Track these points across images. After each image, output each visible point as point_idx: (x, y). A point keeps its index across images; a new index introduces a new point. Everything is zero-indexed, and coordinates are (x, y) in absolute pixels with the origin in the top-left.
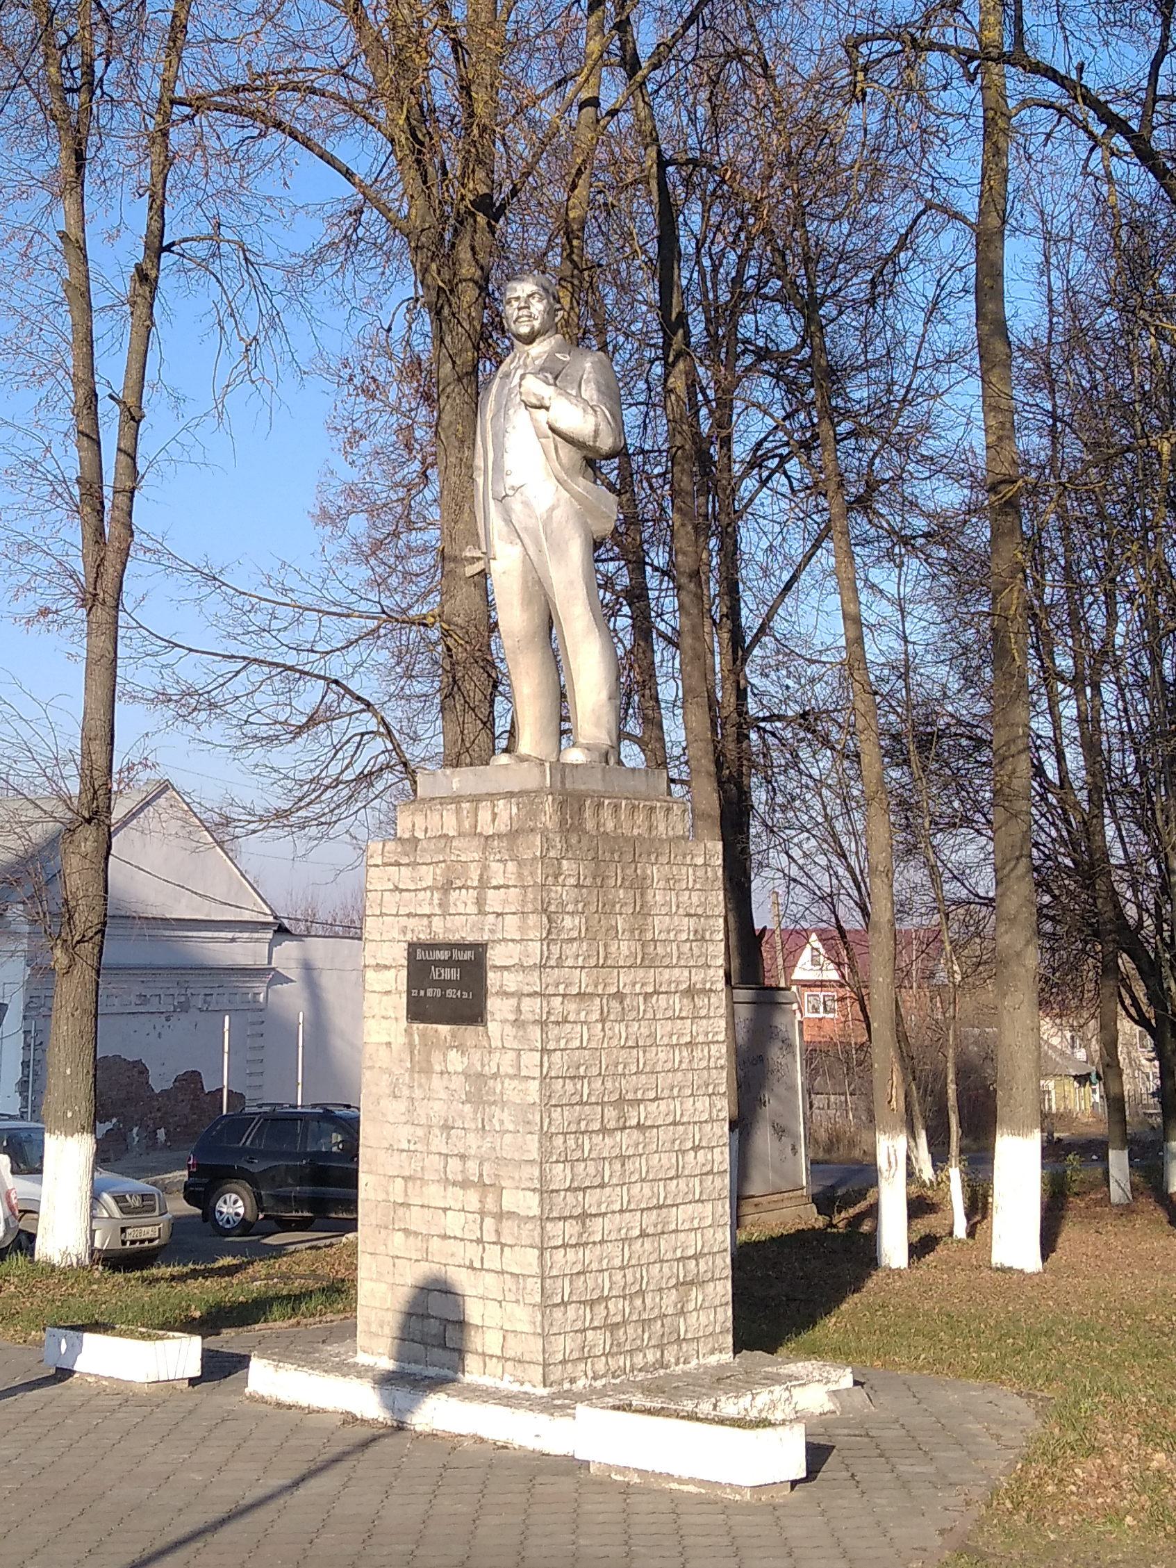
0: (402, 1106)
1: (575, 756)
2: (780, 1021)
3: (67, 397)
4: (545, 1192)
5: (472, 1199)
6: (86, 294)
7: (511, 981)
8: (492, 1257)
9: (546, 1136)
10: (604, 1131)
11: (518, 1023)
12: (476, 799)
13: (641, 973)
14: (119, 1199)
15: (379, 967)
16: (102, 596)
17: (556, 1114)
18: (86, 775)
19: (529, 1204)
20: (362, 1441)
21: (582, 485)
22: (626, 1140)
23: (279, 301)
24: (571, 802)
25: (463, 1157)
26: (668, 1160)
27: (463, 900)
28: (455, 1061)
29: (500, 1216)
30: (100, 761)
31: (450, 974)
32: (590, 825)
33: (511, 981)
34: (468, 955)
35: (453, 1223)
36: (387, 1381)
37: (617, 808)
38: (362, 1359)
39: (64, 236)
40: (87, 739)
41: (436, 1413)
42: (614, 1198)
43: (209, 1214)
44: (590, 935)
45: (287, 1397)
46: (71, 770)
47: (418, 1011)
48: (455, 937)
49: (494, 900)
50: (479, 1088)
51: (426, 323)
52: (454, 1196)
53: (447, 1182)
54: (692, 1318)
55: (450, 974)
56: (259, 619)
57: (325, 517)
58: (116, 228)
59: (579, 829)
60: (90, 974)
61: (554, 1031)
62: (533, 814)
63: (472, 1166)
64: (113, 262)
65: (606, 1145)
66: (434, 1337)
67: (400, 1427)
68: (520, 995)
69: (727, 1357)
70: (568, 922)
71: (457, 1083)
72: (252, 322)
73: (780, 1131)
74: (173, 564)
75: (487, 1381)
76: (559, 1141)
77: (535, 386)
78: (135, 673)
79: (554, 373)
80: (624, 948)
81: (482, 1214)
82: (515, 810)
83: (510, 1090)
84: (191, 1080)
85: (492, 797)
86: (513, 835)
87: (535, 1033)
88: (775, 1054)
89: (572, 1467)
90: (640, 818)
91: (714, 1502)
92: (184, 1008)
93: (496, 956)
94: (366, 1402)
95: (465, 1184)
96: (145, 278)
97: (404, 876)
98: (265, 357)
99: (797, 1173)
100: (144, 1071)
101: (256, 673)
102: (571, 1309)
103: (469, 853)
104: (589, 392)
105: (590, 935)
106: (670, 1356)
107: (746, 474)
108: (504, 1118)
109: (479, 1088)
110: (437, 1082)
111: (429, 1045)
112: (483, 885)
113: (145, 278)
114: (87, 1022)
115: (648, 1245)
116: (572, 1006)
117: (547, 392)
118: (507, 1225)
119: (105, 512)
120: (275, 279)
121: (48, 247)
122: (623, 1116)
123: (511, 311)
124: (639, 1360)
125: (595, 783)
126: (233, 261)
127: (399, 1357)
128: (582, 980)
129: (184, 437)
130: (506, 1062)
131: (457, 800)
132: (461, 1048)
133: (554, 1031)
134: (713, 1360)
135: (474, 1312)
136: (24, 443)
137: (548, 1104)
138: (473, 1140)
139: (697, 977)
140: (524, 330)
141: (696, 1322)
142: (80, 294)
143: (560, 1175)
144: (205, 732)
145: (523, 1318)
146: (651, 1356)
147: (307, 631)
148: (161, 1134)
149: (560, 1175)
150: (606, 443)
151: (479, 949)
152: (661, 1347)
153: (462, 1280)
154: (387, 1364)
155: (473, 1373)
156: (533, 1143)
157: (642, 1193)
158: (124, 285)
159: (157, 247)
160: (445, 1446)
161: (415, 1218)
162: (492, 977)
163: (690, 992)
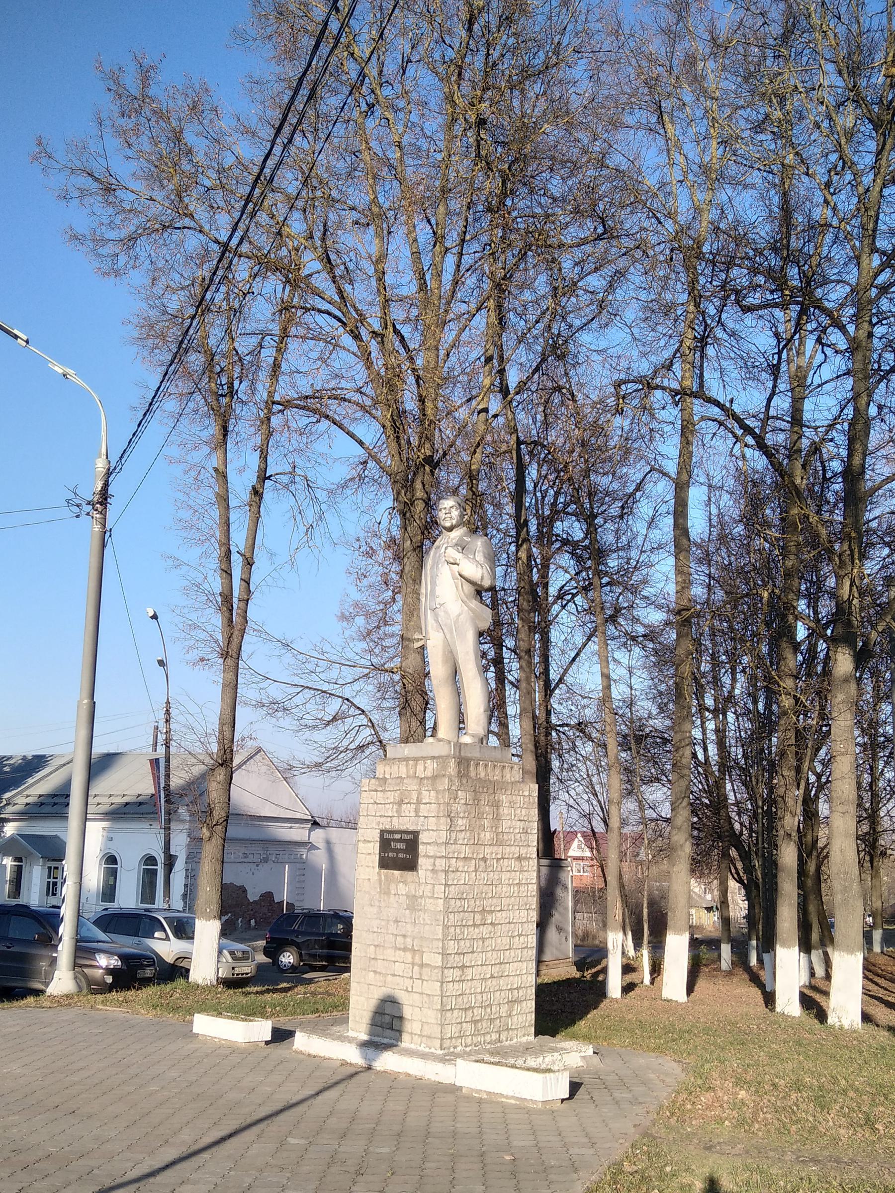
0: (375, 910)
1: (466, 739)
3: (216, 552)
4: (445, 954)
5: (409, 956)
6: (226, 500)
7: (432, 850)
9: (446, 927)
10: (474, 925)
12: (416, 760)
13: (495, 848)
14: (232, 953)
16: (231, 653)
17: (451, 916)
19: (438, 960)
21: (475, 604)
22: (486, 930)
24: (463, 762)
25: (404, 936)
27: (408, 810)
28: (402, 889)
29: (422, 966)
31: (402, 846)
32: (473, 774)
34: (409, 837)
35: (398, 968)
36: (364, 1045)
38: (351, 1034)
39: (216, 470)
40: (222, 724)
41: (388, 1061)
42: (479, 959)
43: (276, 962)
45: (313, 1052)
47: (385, 864)
48: (403, 828)
53: (396, 948)
55: (402, 846)
56: (310, 666)
57: (343, 617)
59: (467, 775)
61: (451, 875)
62: (444, 767)
64: (241, 484)
65: (475, 932)
66: (387, 1024)
67: (369, 1068)
68: (435, 857)
69: (532, 1038)
70: (460, 822)
71: (403, 899)
73: (560, 929)
76: (452, 930)
77: (453, 554)
79: (462, 547)
80: (487, 836)
81: (413, 964)
82: (435, 765)
83: (429, 904)
86: (434, 778)
88: (559, 892)
89: (453, 1089)
90: (498, 771)
91: (523, 1108)
92: (266, 860)
93: (423, 838)
94: (353, 1056)
95: (405, 949)
96: (257, 493)
100: (245, 891)
101: (308, 694)
103: (413, 786)
104: (480, 557)
112: (419, 802)
113: (257, 493)
114: (218, 867)
115: (494, 981)
116: (460, 864)
118: (426, 971)
121: (208, 475)
122: (484, 919)
124: (488, 1038)
126: (300, 484)
127: (371, 1034)
128: (466, 851)
129: (274, 574)
131: (407, 759)
132: (405, 883)
133: (451, 875)
134: (524, 1039)
137: (447, 911)
138: (409, 927)
139: (523, 851)
140: (448, 524)
142: (223, 500)
143: (452, 946)
145: (432, 1016)
146: (494, 1036)
149: (452, 946)
151: (416, 834)
152: (499, 1032)
153: (402, 997)
154: (365, 1037)
155: (406, 1042)
157: (492, 957)
159: (263, 477)
160: (392, 1079)
161: (380, 966)
163: (520, 858)
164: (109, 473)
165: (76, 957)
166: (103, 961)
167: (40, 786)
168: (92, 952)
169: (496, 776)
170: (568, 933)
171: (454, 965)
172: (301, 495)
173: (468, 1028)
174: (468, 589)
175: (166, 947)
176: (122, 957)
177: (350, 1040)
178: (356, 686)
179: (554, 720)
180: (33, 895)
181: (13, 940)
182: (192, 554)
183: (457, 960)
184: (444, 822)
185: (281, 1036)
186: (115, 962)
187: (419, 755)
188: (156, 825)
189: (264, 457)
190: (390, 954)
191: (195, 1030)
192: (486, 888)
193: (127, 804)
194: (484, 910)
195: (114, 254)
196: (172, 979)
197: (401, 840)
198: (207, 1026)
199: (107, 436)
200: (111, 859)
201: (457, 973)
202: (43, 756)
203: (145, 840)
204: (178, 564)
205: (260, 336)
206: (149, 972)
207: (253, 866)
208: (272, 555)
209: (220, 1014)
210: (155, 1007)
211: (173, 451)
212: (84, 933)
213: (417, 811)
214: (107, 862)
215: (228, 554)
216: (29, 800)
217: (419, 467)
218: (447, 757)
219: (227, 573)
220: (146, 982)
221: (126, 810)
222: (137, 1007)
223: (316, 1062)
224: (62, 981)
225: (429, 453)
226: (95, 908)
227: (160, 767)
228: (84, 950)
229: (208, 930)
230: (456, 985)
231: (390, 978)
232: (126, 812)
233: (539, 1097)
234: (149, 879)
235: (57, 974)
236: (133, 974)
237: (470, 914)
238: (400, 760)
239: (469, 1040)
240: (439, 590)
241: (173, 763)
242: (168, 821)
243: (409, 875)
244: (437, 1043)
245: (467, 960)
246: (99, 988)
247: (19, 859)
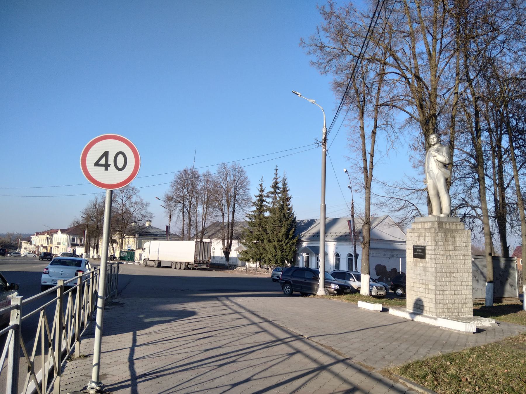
0: (413, 271)
1: (442, 215)
2: (512, 264)
3: (361, 154)
4: (436, 286)
5: (424, 286)
6: (364, 136)
7: (430, 252)
8: (427, 295)
9: (436, 277)
10: (447, 277)
11: (431, 259)
12: (424, 222)
13: (454, 252)
14: (376, 287)
15: (409, 249)
16: (368, 187)
17: (438, 274)
18: (366, 216)
19: (433, 288)
20: (405, 321)
21: (443, 169)
22: (451, 279)
23: (398, 134)
24: (440, 223)
26: (460, 283)
27: (422, 239)
28: (421, 264)
29: (429, 289)
30: (368, 214)
31: (420, 251)
32: (444, 227)
33: (430, 252)
34: (423, 248)
35: (421, 290)
36: (411, 314)
37: (449, 224)
38: (407, 310)
39: (360, 127)
40: (366, 210)
41: (418, 319)
42: (449, 288)
43: (395, 292)
44: (444, 245)
45: (395, 315)
46: (363, 215)
47: (415, 256)
48: (420, 245)
49: (427, 239)
50: (425, 269)
51: (423, 137)
52: (421, 286)
53: (420, 283)
54: (465, 309)
55: (420, 251)
56: (392, 191)
57: (415, 167)
58: (369, 123)
59: (442, 228)
60: (367, 249)
61: (437, 260)
62: (434, 225)
63: (424, 281)
64: (368, 131)
65: (448, 279)
66: (419, 307)
67: (413, 320)
68: (431, 254)
69: (472, 316)
70: (440, 243)
71: (421, 268)
72: (393, 138)
73: (511, 286)
74: (378, 182)
75: (427, 315)
76: (438, 278)
77: (434, 153)
78: (373, 201)
79: (438, 151)
80: (451, 247)
81: (426, 289)
83: (430, 269)
84: (394, 270)
85: (427, 222)
86: (430, 228)
87: (434, 261)
88: (511, 271)
89: (438, 328)
90: (454, 226)
91: (459, 334)
92: (393, 256)
93: (427, 248)
94: (408, 317)
95: (423, 284)
96: (374, 133)
97: (412, 235)
98: (396, 144)
99: (516, 294)
100: (385, 267)
101: (392, 200)
102: (441, 305)
103: (423, 231)
104: (444, 154)
105: (444, 245)
106: (460, 314)
107: (504, 154)
108: (428, 274)
109: (425, 269)
110: (418, 268)
111: (417, 262)
112: (425, 236)
113: (374, 133)
114: (367, 257)
115: (456, 296)
116: (441, 257)
117: (436, 154)
118: (430, 291)
119: (367, 172)
120: (397, 130)
121: (358, 129)
122: (450, 275)
123: (431, 140)
124: (454, 314)
125: (446, 220)
126: (389, 127)
127: (414, 310)
128: (443, 253)
129: (382, 159)
130: (429, 265)
131: (421, 222)
132: (422, 263)
133: (437, 260)
134: (469, 316)
135: (425, 304)
136: (354, 162)
137: (436, 272)
138: (424, 277)
139: (466, 253)
140: (433, 143)
141: (465, 310)
142: (363, 136)
143: (439, 283)
144: (383, 210)
145: (433, 305)
146: (456, 314)
147: (400, 193)
148: (389, 279)
149: (439, 283)
150: (447, 162)
151: (425, 247)
152: (458, 313)
153: (423, 299)
154: (412, 311)
155: (425, 313)
156: (433, 278)
157: (455, 288)
158: (370, 134)
159: (376, 127)
160: (419, 323)
161: (415, 289)
162: (427, 252)
163: (464, 255)
164: (326, 133)
165: (325, 284)
166: (333, 286)
167: (312, 230)
168: (330, 283)
169: (454, 227)
170: (515, 287)
171: (440, 289)
172: (389, 131)
173: (446, 310)
174: (440, 164)
175: (354, 284)
176: (339, 285)
177: (406, 312)
178: (410, 197)
179: (507, 201)
180: (313, 266)
181: (306, 278)
182: (353, 155)
183: (441, 288)
184: (434, 243)
185: (385, 310)
186: (337, 287)
187: (423, 221)
188: (351, 243)
189: (376, 121)
190: (418, 285)
191: (359, 306)
192: (451, 265)
193: (341, 236)
194: (450, 272)
195: (323, 67)
196: (355, 293)
197: (420, 249)
198: (362, 305)
199: (325, 121)
200: (337, 255)
201: (441, 292)
202: (314, 220)
203: (347, 249)
204: (349, 159)
205: (369, 86)
206: (348, 291)
207: (388, 259)
208: (381, 152)
209: (366, 302)
210: (348, 300)
211: (346, 122)
212: (328, 277)
213: (425, 239)
214: (336, 256)
215: (365, 154)
216: (310, 235)
217: (431, 117)
218: (435, 221)
219: (365, 160)
220: (346, 294)
221: (342, 238)
222: (344, 299)
223: (395, 317)
224: (321, 291)
225: (434, 112)
226: (332, 269)
227: (351, 223)
228: (327, 283)
229: (365, 278)
230: (441, 296)
231: (418, 293)
232: (341, 239)
233: (464, 331)
234: (350, 261)
235: (319, 289)
236: (343, 290)
237: (445, 274)
238: (419, 222)
239: (447, 314)
240: (430, 166)
241: (356, 222)
242: (355, 242)
243: (423, 260)
244: (435, 314)
245: (444, 288)
246: (331, 293)
247: (308, 254)
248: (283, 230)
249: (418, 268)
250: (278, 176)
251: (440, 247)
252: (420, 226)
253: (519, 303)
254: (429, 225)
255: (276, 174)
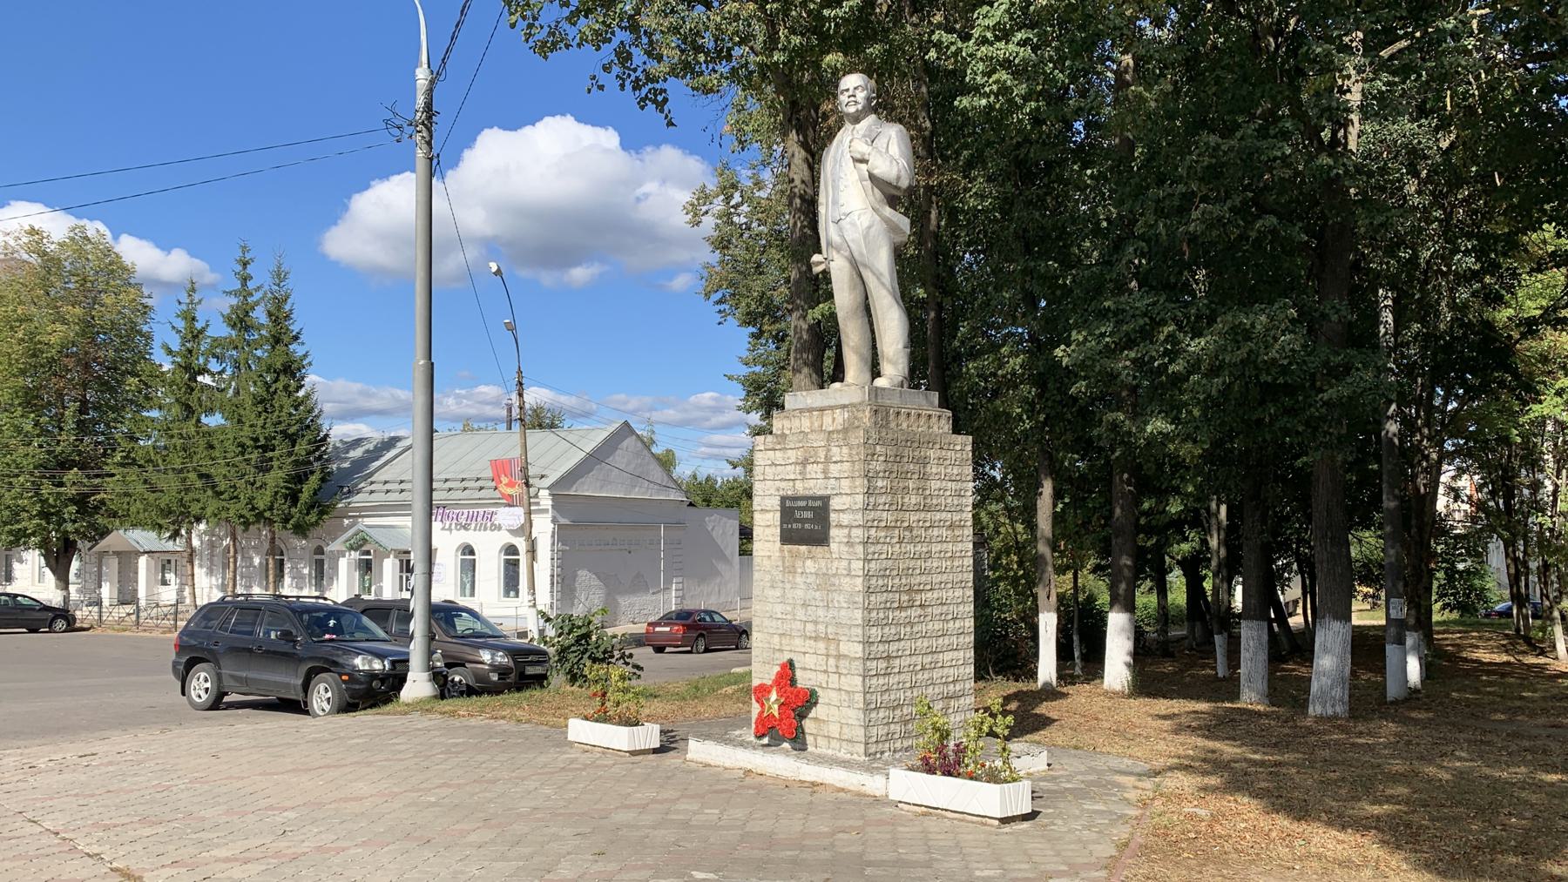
5: (821, 645)
7: (845, 519)
11: (849, 544)
12: (822, 410)
19: (857, 650)
22: (915, 612)
29: (839, 657)
31: (808, 515)
34: (818, 503)
44: (892, 492)
47: (788, 538)
49: (834, 469)
50: (826, 582)
53: (806, 637)
55: (808, 515)
86: (845, 430)
93: (835, 503)
110: (799, 579)
112: (828, 460)
131: (810, 410)
137: (868, 591)
138: (821, 612)
151: (826, 500)
171: (878, 659)
187: (818, 404)
237: (892, 595)
240: (844, 197)
243: (818, 551)
244: (861, 748)
248: (276, 477)
249: (799, 579)
250: (251, 285)
251: (882, 500)
252: (805, 424)
253: (300, 698)
254: (840, 417)
255: (245, 280)
